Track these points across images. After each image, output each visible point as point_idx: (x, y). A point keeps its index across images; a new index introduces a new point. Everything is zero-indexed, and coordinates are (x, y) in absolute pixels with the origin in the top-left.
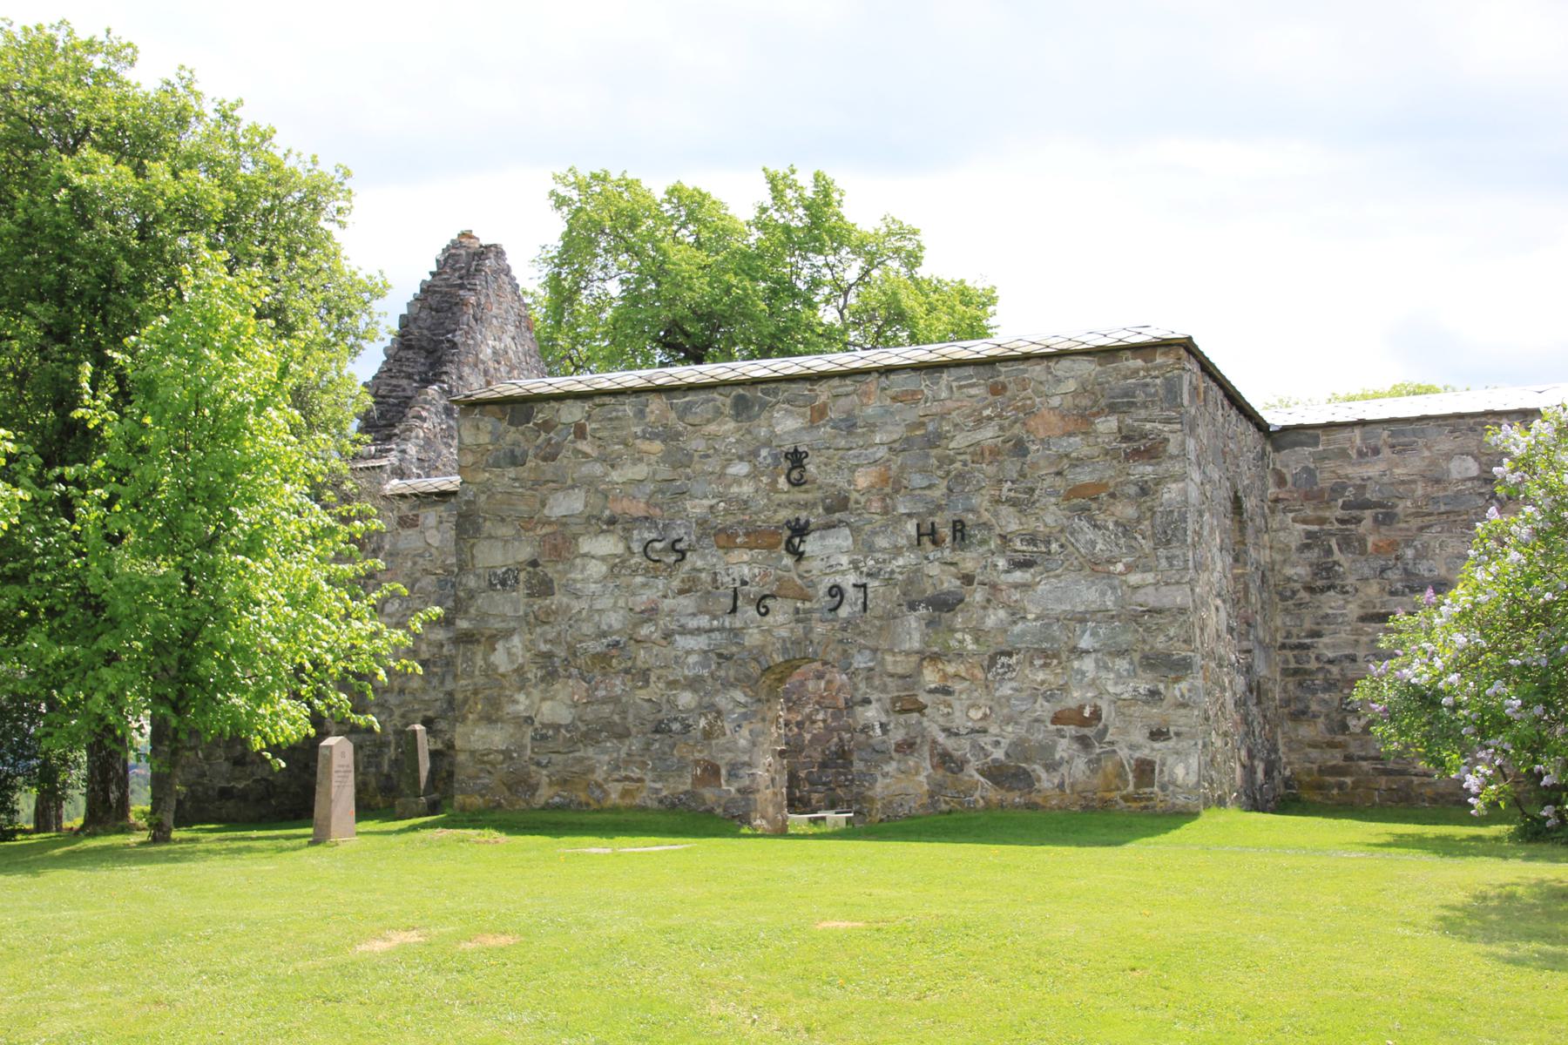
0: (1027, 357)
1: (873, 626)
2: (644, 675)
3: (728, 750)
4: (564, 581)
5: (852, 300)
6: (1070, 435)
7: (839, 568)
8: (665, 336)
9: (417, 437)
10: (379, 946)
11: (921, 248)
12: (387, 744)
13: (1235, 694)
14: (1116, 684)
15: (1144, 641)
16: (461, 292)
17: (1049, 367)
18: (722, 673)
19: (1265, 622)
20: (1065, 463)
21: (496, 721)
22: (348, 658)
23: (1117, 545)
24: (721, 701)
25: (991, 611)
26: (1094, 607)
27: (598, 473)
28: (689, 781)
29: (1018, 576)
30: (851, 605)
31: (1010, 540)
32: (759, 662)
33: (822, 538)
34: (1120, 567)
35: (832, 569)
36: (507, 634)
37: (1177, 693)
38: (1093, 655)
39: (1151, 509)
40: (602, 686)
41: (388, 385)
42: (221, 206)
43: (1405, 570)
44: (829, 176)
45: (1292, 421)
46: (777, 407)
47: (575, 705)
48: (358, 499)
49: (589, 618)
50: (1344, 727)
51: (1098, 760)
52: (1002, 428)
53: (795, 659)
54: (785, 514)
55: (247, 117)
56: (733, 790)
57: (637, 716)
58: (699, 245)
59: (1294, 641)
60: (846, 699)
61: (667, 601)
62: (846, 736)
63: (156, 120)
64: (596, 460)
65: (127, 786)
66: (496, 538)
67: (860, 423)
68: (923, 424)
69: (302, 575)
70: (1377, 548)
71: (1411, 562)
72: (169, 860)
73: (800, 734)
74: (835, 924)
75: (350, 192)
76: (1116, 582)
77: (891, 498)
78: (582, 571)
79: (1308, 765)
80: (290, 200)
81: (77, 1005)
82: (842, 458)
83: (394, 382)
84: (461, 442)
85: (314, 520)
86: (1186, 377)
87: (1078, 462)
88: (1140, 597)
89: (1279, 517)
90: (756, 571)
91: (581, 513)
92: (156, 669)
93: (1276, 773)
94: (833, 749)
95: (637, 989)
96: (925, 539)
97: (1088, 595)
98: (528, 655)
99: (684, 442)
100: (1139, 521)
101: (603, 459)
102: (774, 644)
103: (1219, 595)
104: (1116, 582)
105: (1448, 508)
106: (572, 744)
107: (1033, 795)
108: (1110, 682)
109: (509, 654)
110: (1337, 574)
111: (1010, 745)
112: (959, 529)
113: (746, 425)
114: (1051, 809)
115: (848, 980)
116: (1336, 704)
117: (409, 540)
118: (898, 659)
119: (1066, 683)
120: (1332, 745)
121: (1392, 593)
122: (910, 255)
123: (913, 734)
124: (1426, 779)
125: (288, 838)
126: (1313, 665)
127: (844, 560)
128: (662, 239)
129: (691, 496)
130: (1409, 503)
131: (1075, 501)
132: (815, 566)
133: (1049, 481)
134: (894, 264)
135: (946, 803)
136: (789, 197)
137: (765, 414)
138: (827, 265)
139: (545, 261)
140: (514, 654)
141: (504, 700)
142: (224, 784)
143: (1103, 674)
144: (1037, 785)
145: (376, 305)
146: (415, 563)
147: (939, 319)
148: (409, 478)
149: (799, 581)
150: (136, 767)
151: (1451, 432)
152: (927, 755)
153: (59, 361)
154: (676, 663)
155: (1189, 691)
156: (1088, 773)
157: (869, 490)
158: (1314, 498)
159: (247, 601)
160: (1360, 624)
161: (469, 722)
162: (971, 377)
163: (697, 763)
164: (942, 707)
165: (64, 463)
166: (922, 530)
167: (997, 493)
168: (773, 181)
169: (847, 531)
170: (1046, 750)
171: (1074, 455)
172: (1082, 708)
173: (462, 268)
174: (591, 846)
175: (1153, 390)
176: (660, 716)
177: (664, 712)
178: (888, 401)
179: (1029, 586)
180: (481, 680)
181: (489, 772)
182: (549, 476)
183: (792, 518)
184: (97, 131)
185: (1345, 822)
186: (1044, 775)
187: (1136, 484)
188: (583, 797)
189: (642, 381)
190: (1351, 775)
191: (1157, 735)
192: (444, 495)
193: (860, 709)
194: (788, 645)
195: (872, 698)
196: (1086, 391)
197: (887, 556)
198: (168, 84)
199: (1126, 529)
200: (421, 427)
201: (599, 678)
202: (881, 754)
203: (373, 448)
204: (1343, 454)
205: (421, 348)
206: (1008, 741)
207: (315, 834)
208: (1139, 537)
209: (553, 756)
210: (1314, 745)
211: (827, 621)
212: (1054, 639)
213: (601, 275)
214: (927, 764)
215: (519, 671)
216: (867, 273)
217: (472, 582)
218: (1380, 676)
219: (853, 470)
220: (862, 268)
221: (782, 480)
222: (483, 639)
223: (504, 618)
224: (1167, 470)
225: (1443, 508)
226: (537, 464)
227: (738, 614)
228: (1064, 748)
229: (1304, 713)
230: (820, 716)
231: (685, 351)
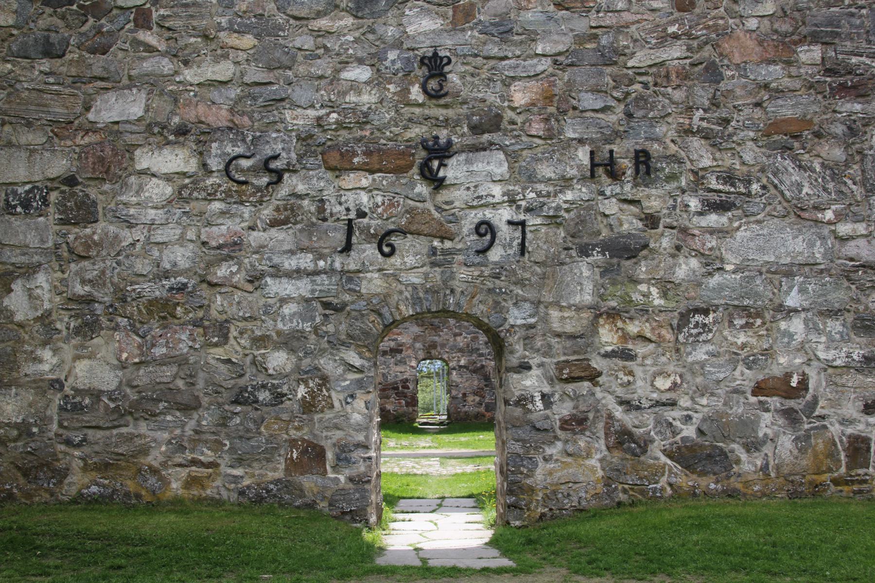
1: (533, 273)
2: (222, 330)
3: (337, 427)
4: (112, 206)
6: (770, 62)
7: (490, 200)
14: (828, 348)
15: (858, 301)
18: (331, 328)
21: (9, 386)
24: (328, 365)
25: (681, 260)
26: (801, 259)
28: (282, 466)
29: (713, 219)
30: (504, 247)
31: (703, 177)
32: (380, 315)
34: (829, 215)
36: (30, 271)
38: (803, 315)
40: (162, 341)
47: (123, 366)
49: (146, 253)
51: (807, 437)
52: (689, 49)
54: (416, 132)
56: (342, 478)
57: (208, 383)
61: (255, 234)
64: (164, 54)
66: (19, 147)
68: (595, 37)
76: (826, 231)
77: (558, 121)
78: (138, 193)
82: (493, 68)
87: (778, 93)
88: (850, 249)
90: (379, 199)
91: (140, 120)
96: (600, 171)
98: (58, 299)
99: (284, 37)
100: (847, 165)
102: (401, 292)
107: (732, 480)
108: (821, 347)
109: (30, 296)
112: (642, 159)
118: (566, 315)
119: (771, 347)
123: (583, 407)
127: (497, 191)
131: (776, 137)
132: (458, 196)
133: (747, 111)
135: (625, 491)
140: (38, 298)
141: (21, 357)
143: (813, 337)
144: (736, 468)
149: (436, 215)
152: (601, 434)
154: (266, 313)
156: (796, 452)
157: (527, 109)
163: (293, 443)
164: (621, 375)
166: (597, 160)
167: (687, 122)
169: (501, 156)
171: (773, 85)
172: (788, 376)
175: (858, 22)
176: (242, 382)
179: (727, 232)
182: (97, 71)
183: (427, 136)
186: (744, 456)
193: (515, 376)
194: (421, 295)
197: (551, 189)
199: (835, 171)
201: (158, 331)
208: (849, 182)
209: (90, 432)
211: (473, 265)
215: (45, 319)
219: (508, 82)
223: (24, 248)
226: (81, 56)
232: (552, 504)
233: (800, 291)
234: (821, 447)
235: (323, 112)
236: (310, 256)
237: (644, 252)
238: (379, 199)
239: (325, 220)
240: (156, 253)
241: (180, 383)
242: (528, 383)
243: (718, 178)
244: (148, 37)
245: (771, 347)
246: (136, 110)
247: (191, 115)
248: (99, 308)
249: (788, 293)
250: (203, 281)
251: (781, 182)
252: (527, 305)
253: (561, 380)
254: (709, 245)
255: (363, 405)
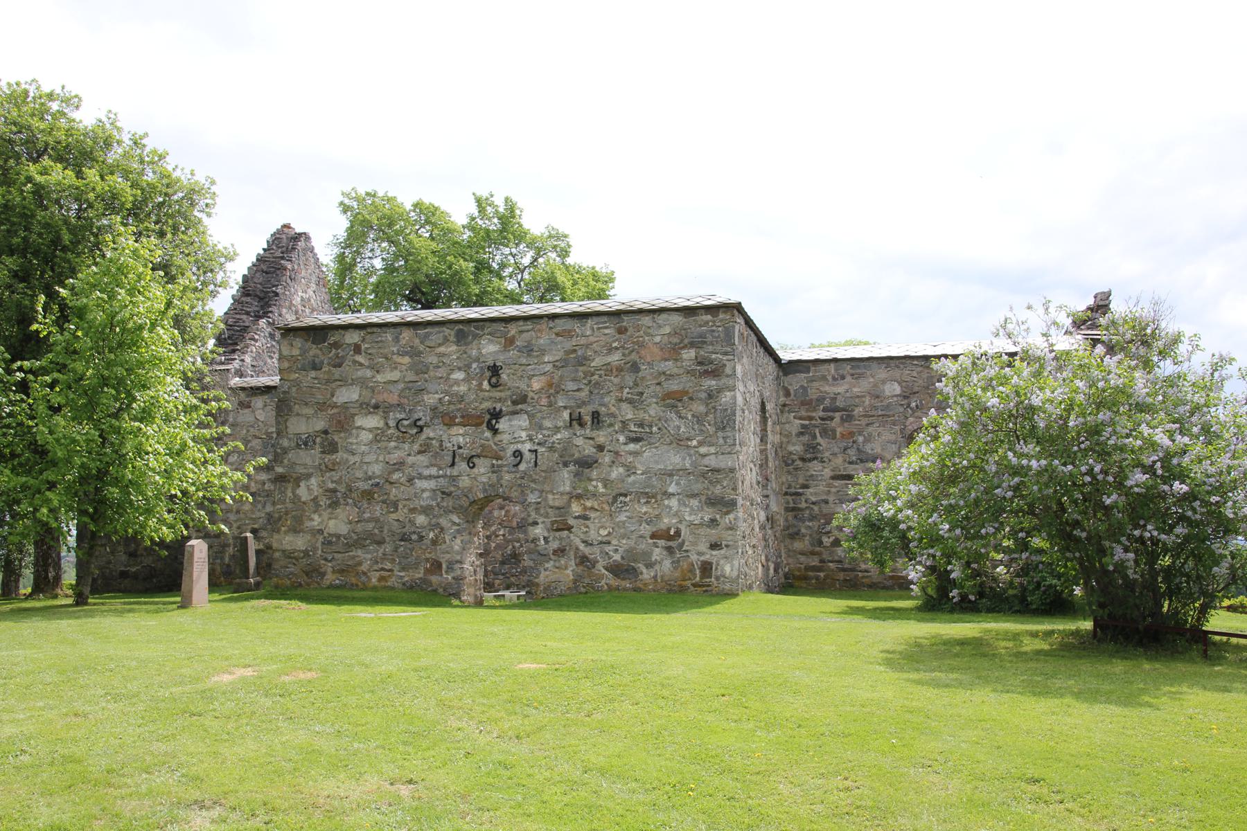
0: (641, 311)
1: (541, 476)
4: (345, 444)
5: (526, 276)
6: (666, 360)
7: (520, 439)
8: (409, 294)
9: (252, 352)
10: (226, 678)
11: (569, 246)
12: (229, 545)
13: (759, 522)
14: (691, 514)
15: (708, 489)
16: (282, 262)
17: (654, 318)
18: (445, 504)
19: (777, 479)
20: (663, 378)
21: (299, 532)
22: (205, 489)
23: (693, 429)
24: (444, 522)
25: (614, 468)
26: (678, 467)
27: (369, 376)
28: (422, 571)
29: (632, 447)
30: (527, 463)
31: (627, 425)
32: (468, 497)
33: (510, 420)
34: (695, 443)
35: (516, 441)
36: (308, 476)
37: (727, 521)
38: (677, 497)
39: (714, 408)
40: (368, 510)
41: (234, 318)
42: (131, 199)
43: (858, 449)
44: (514, 199)
45: (795, 357)
46: (484, 337)
47: (350, 522)
48: (213, 389)
49: (361, 467)
50: (820, 543)
51: (678, 561)
52: (624, 355)
53: (491, 495)
54: (487, 405)
55: (150, 144)
56: (450, 577)
57: (389, 531)
58: (432, 238)
59: (793, 490)
60: (517, 522)
61: (410, 458)
62: (517, 545)
63: (90, 143)
64: (368, 367)
65: (60, 568)
67: (535, 349)
68: (575, 351)
69: (177, 435)
70: (843, 435)
71: (861, 445)
72: (86, 616)
73: (489, 543)
74: (527, 665)
75: (214, 194)
76: (692, 452)
77: (554, 397)
78: (356, 438)
79: (799, 565)
80: (175, 197)
81: (22, 716)
82: (523, 370)
83: (238, 316)
84: (280, 354)
85: (185, 401)
86: (737, 327)
88: (706, 461)
89: (786, 415)
90: (468, 440)
91: (357, 401)
92: (80, 493)
93: (780, 570)
94: (509, 552)
95: (401, 709)
96: (574, 423)
97: (675, 459)
98: (321, 490)
100: (706, 414)
101: (371, 367)
103: (752, 461)
104: (692, 452)
105: (883, 413)
106: (349, 547)
109: (309, 489)
110: (819, 451)
111: (624, 551)
112: (596, 416)
113: (463, 348)
114: (649, 591)
115: (541, 704)
116: (816, 529)
117: (245, 416)
119: (660, 514)
120: (813, 553)
121: (851, 463)
122: (562, 250)
123: (564, 544)
124: (866, 574)
125: (164, 603)
126: (804, 505)
127: (524, 434)
128: (410, 234)
129: (427, 392)
130: (861, 410)
131: (668, 401)
132: (505, 438)
133: (652, 388)
134: (554, 255)
135: (584, 587)
136: (489, 211)
137: (476, 342)
138: (511, 254)
139: (335, 244)
140: (312, 489)
141: (304, 518)
142: (123, 569)
143: (683, 509)
144: (640, 577)
145: (229, 266)
146: (248, 431)
147: (580, 290)
148: (246, 377)
149: (495, 447)
150: (67, 556)
151: (886, 367)
152: (573, 557)
153: (22, 294)
154: (415, 497)
155: (735, 519)
156: (672, 569)
157: (539, 392)
158: (806, 405)
159: (140, 452)
160: (831, 481)
161: (282, 533)
162: (606, 322)
163: (427, 560)
165: (23, 359)
166: (573, 417)
168: (479, 201)
169: (526, 417)
170: (647, 554)
171: (668, 372)
172: (669, 529)
173: (283, 247)
174: (361, 612)
175: (717, 335)
176: (404, 530)
177: (407, 528)
178: (554, 336)
180: (290, 506)
181: (294, 564)
182: (337, 376)
184: (52, 149)
185: (824, 600)
186: (645, 571)
187: (705, 392)
188: (354, 580)
189: (398, 318)
190: (823, 571)
191: (714, 546)
192: (268, 389)
195: (539, 521)
196: (676, 333)
197: (550, 433)
198: (100, 121)
199: (699, 419)
200: (254, 346)
201: (366, 506)
202: (544, 556)
203: (223, 358)
204: (824, 378)
205: (256, 296)
206: (623, 549)
207: (182, 602)
209: (335, 554)
210: (802, 553)
211: (512, 472)
212: (653, 487)
213: (371, 255)
214: (573, 563)
215: (315, 500)
216: (536, 260)
217: (285, 443)
218: (849, 512)
219: (530, 377)
220: (533, 257)
221: (485, 383)
222: (292, 480)
224: (724, 384)
225: (880, 413)
227: (455, 467)
228: (657, 554)
229: (797, 534)
230: (501, 533)
231: (422, 304)
232: (548, 592)
233: (676, 484)
234: (685, 566)
235: (442, 396)
236: (436, 468)
237: (596, 465)
238: (468, 440)
239: (443, 450)
240: (365, 468)
241: (376, 531)
242: (537, 531)
243: (635, 425)
244: (360, 358)
245: (660, 514)
246: (355, 397)
247: (380, 398)
248: (339, 495)
249: (670, 485)
250: (387, 481)
251: (669, 426)
252: (537, 492)
253: (553, 530)
254: (629, 460)
255: (459, 542)
